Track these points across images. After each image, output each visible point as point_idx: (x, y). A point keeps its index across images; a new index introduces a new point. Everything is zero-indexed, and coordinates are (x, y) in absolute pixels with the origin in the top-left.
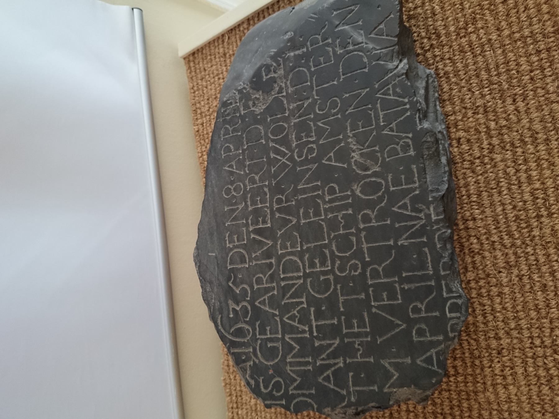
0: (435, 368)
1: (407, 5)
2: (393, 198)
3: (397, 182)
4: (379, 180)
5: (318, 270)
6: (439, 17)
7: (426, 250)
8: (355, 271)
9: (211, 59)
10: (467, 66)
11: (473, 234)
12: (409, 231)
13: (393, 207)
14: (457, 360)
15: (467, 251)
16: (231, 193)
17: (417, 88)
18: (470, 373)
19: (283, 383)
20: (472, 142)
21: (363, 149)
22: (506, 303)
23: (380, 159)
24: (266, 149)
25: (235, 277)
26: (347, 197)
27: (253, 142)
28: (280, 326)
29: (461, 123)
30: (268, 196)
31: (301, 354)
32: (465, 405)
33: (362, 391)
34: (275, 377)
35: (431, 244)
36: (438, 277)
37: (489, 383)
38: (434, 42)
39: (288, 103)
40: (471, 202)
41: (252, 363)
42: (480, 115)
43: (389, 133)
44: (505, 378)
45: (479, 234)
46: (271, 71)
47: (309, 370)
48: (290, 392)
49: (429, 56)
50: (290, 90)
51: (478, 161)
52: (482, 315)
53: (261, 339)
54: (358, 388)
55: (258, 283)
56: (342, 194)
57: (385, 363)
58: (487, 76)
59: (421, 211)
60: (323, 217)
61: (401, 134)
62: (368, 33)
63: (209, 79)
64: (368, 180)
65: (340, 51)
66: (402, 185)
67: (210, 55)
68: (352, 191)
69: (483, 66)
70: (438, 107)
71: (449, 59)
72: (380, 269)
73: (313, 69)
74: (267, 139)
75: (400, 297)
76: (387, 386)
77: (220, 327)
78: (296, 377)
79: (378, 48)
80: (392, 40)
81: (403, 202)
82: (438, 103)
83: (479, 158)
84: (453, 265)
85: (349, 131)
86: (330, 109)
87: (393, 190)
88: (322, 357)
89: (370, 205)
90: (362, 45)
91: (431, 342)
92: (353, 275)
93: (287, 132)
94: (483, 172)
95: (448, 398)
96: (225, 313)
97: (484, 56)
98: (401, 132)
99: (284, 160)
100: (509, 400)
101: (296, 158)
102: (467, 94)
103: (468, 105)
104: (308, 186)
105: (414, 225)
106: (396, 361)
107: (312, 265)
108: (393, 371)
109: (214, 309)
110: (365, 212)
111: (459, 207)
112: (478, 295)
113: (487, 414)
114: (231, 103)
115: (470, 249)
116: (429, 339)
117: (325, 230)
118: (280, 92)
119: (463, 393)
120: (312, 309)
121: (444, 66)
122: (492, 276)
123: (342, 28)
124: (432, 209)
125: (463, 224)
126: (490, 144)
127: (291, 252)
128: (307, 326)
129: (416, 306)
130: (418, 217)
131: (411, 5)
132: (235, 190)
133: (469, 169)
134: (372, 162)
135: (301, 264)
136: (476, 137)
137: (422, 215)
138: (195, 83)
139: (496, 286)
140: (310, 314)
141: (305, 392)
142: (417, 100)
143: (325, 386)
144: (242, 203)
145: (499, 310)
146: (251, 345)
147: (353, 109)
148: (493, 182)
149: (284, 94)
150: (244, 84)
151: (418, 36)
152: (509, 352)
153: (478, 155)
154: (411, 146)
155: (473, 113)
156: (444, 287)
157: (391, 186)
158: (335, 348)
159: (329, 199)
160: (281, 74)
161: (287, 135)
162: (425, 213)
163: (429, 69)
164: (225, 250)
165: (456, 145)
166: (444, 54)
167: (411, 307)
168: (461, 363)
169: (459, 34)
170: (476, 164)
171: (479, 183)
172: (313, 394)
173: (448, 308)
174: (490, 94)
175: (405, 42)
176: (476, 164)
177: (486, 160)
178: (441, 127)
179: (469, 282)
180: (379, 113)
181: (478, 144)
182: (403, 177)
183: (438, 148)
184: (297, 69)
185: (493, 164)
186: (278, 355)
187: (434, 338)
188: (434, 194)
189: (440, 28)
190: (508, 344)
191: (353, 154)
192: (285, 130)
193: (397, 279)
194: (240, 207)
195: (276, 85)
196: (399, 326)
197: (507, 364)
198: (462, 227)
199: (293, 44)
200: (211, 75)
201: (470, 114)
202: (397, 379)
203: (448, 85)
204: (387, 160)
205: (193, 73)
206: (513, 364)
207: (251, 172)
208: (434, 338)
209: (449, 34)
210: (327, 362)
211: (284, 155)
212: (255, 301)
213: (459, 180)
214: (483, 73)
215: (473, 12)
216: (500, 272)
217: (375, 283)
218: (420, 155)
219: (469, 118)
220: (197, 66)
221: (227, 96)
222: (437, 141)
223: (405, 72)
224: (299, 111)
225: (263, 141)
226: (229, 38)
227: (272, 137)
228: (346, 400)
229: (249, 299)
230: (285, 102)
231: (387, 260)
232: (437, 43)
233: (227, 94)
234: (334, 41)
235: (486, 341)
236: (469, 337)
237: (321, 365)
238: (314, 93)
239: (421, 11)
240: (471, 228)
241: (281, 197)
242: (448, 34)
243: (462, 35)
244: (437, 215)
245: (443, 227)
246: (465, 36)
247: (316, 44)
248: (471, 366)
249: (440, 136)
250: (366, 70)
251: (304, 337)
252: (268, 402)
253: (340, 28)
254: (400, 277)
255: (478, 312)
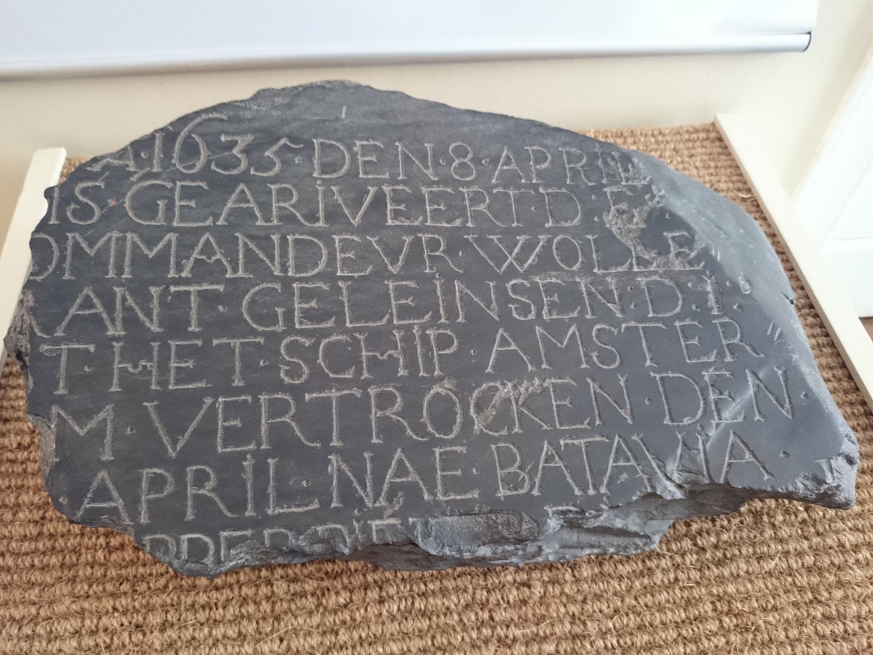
0: (87, 505)
1: (779, 512)
2: (420, 453)
3: (449, 461)
4: (456, 429)
5: (296, 305)
6: (755, 566)
7: (315, 506)
8: (287, 373)
9: (709, 167)
10: (661, 609)
11: (354, 598)
12: (355, 476)
13: (403, 451)
14: (134, 553)
15: (325, 584)
16: (458, 157)
17: (627, 515)
18: (108, 573)
19: (89, 222)
20: (521, 608)
21: (517, 403)
22: (225, 646)
23: (496, 434)
24: (534, 227)
25: (296, 152)
26: (430, 369)
27: (550, 205)
28: (195, 225)
29: (557, 591)
30: (445, 225)
31: (138, 259)
32: (54, 560)
33: (58, 367)
34: (102, 208)
35: (324, 514)
36: (258, 524)
37: (86, 605)
38: (708, 555)
39: (618, 275)
40: (413, 597)
41: (132, 169)
42: (568, 626)
43: (544, 454)
44: (93, 633)
45: (354, 608)
46: (682, 247)
47: (107, 273)
48: (69, 235)
49: (684, 544)
50: (642, 280)
51: (486, 616)
52: (208, 603)
53: (173, 190)
54: (64, 358)
55: (280, 191)
56: (436, 360)
57: (107, 413)
58: (639, 644)
59: (390, 500)
60: (395, 322)
61: (539, 476)
62: (737, 430)
63: (675, 163)
64: (458, 408)
65: (707, 375)
66: (443, 470)
67: (716, 167)
68: (440, 379)
69: (657, 638)
70: (588, 551)
71: (677, 580)
72: (286, 419)
73: (677, 324)
74: (554, 232)
75: (228, 450)
76: (62, 413)
77: (204, 116)
78: (96, 247)
79: (708, 446)
80: (720, 473)
81: (410, 469)
82: (596, 551)
83: (492, 618)
84: (281, 553)
85: (553, 381)
86: (600, 349)
87: (434, 452)
88: (128, 297)
89: (411, 410)
90: (716, 418)
91: (137, 500)
92: (280, 368)
93: (563, 269)
94: (464, 624)
95: (69, 531)
96: (230, 128)
97: (675, 641)
98: (543, 475)
99: (510, 259)
100: (52, 637)
101: (513, 282)
102: (609, 607)
103: (588, 607)
104: (458, 300)
105: (364, 487)
106: (108, 433)
107: (306, 295)
108: (89, 427)
109: (239, 107)
110: (399, 400)
111: (406, 574)
112: (244, 599)
113: (33, 597)
114: (626, 170)
115: (328, 590)
116: (143, 498)
117: (371, 324)
118: (641, 261)
119: (74, 559)
120: (221, 288)
121: (663, 570)
122: (276, 625)
123: (750, 383)
124: (392, 521)
125: (375, 582)
126: (515, 640)
127: (336, 259)
128: (190, 276)
129: (208, 479)
130: (380, 495)
131: (780, 518)
132: (463, 165)
133: (473, 599)
134: (491, 418)
135: (309, 274)
136: (530, 615)
137: (382, 502)
138: (669, 138)
139: (258, 631)
140: (212, 283)
141: (68, 260)
142: (601, 510)
143: (74, 300)
144: (436, 175)
145: (214, 632)
146: (164, 169)
147: (595, 393)
148: (445, 641)
149: (636, 269)
150: (661, 197)
151: (722, 527)
152: (137, 645)
153: (497, 618)
154: (515, 493)
155: (574, 615)
156: (239, 533)
157: (442, 450)
158: (142, 324)
159: (428, 336)
160: (673, 264)
161: (557, 268)
162: (385, 509)
163: (661, 542)
164: (349, 137)
165: (518, 579)
166: (685, 571)
167: (208, 470)
168: (127, 559)
169: (719, 601)
170: (480, 613)
171: (445, 615)
172: (63, 275)
173: (199, 538)
174: (606, 647)
175: (715, 499)
176: (480, 613)
177: (486, 632)
178: (550, 552)
179: (269, 583)
180: (583, 438)
181: (516, 619)
182: (459, 473)
183: (507, 541)
184: (679, 295)
185: (478, 643)
186: (140, 217)
187: (144, 508)
188: (419, 528)
189: (733, 567)
190: (152, 643)
191: (510, 385)
192: (566, 264)
193: (264, 447)
194: (430, 173)
195: (653, 254)
196: (174, 442)
197: (115, 638)
198: (370, 579)
199: (728, 291)
200: (681, 166)
201: (573, 609)
202: (73, 431)
203: (629, 573)
204: (493, 447)
205: (686, 136)
206: (116, 649)
207: (495, 198)
208: (144, 508)
209: (722, 583)
210: (118, 306)
211: (521, 260)
212: (246, 183)
213: (455, 579)
214: (646, 638)
215: (757, 629)
216: (282, 640)
217: (261, 407)
218: (496, 507)
219: (565, 607)
220: (698, 144)
221: (641, 165)
222: (520, 541)
223: (658, 493)
224: (600, 293)
225: (550, 224)
226: (743, 200)
227: (555, 241)
228: (44, 336)
229: (252, 172)
230: (620, 269)
231: (302, 432)
232: (707, 560)
233: (644, 164)
234: (727, 366)
235: (162, 606)
236: (172, 578)
237: (115, 294)
238: (633, 324)
239: (767, 536)
240: (366, 594)
241: (442, 249)
242: (721, 580)
243: (718, 605)
244: (380, 531)
245: (356, 539)
246: (715, 610)
247: (723, 332)
248: (119, 576)
249: (531, 548)
250: (667, 421)
251: (169, 269)
252: (56, 194)
253: (750, 379)
254: (268, 454)
255: (215, 596)
